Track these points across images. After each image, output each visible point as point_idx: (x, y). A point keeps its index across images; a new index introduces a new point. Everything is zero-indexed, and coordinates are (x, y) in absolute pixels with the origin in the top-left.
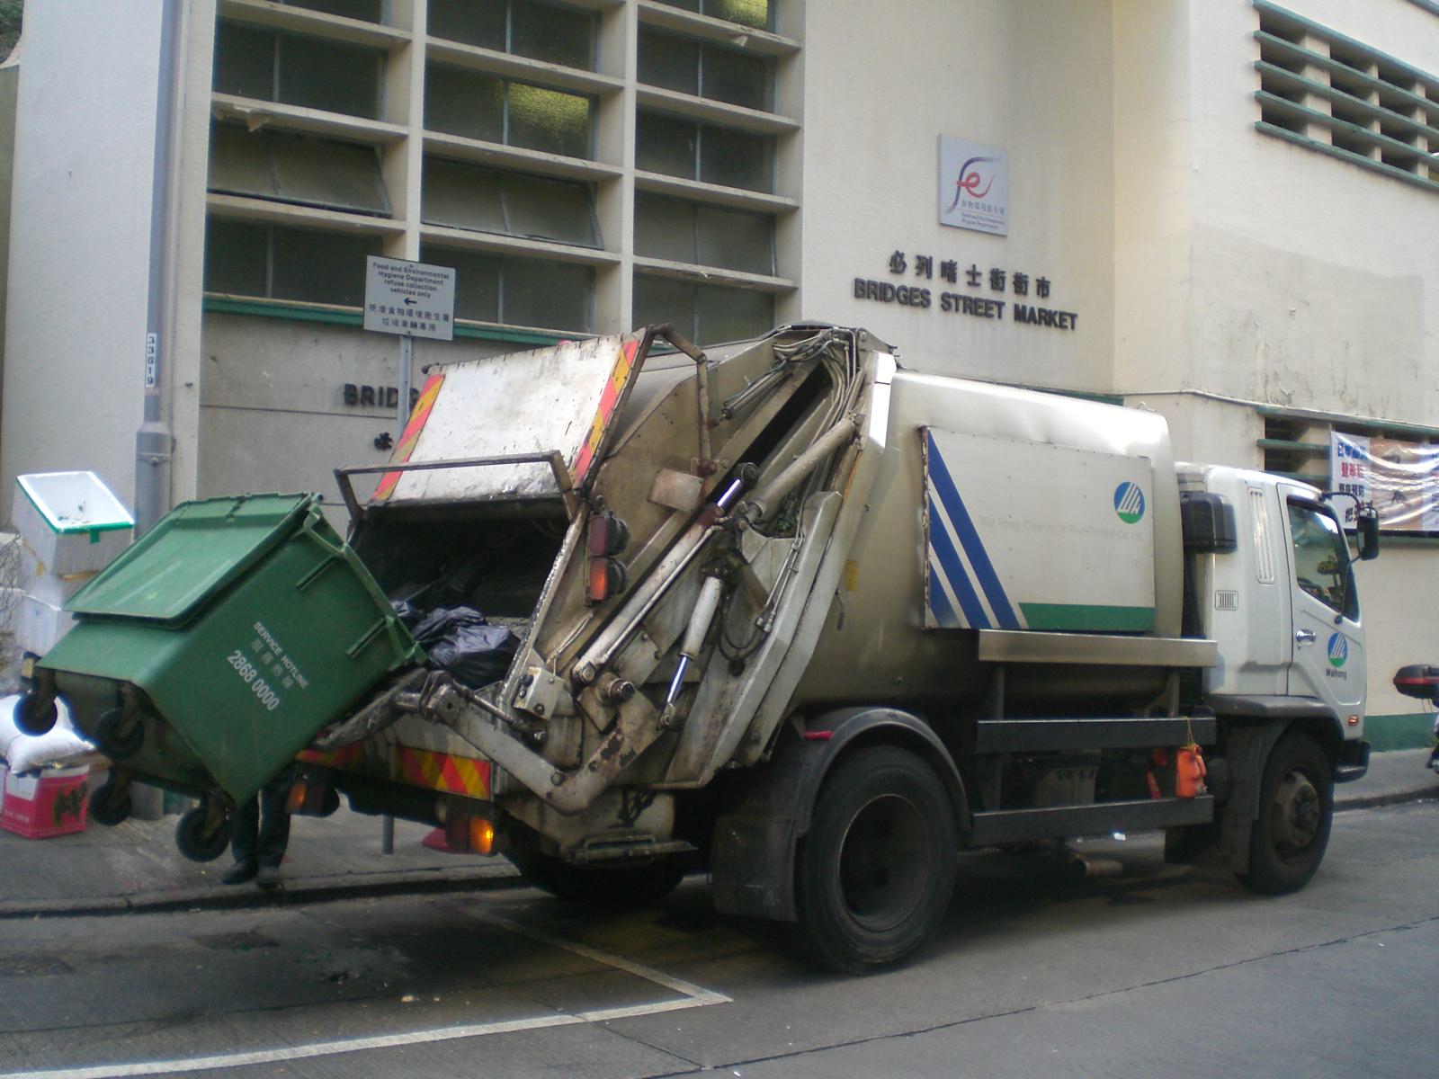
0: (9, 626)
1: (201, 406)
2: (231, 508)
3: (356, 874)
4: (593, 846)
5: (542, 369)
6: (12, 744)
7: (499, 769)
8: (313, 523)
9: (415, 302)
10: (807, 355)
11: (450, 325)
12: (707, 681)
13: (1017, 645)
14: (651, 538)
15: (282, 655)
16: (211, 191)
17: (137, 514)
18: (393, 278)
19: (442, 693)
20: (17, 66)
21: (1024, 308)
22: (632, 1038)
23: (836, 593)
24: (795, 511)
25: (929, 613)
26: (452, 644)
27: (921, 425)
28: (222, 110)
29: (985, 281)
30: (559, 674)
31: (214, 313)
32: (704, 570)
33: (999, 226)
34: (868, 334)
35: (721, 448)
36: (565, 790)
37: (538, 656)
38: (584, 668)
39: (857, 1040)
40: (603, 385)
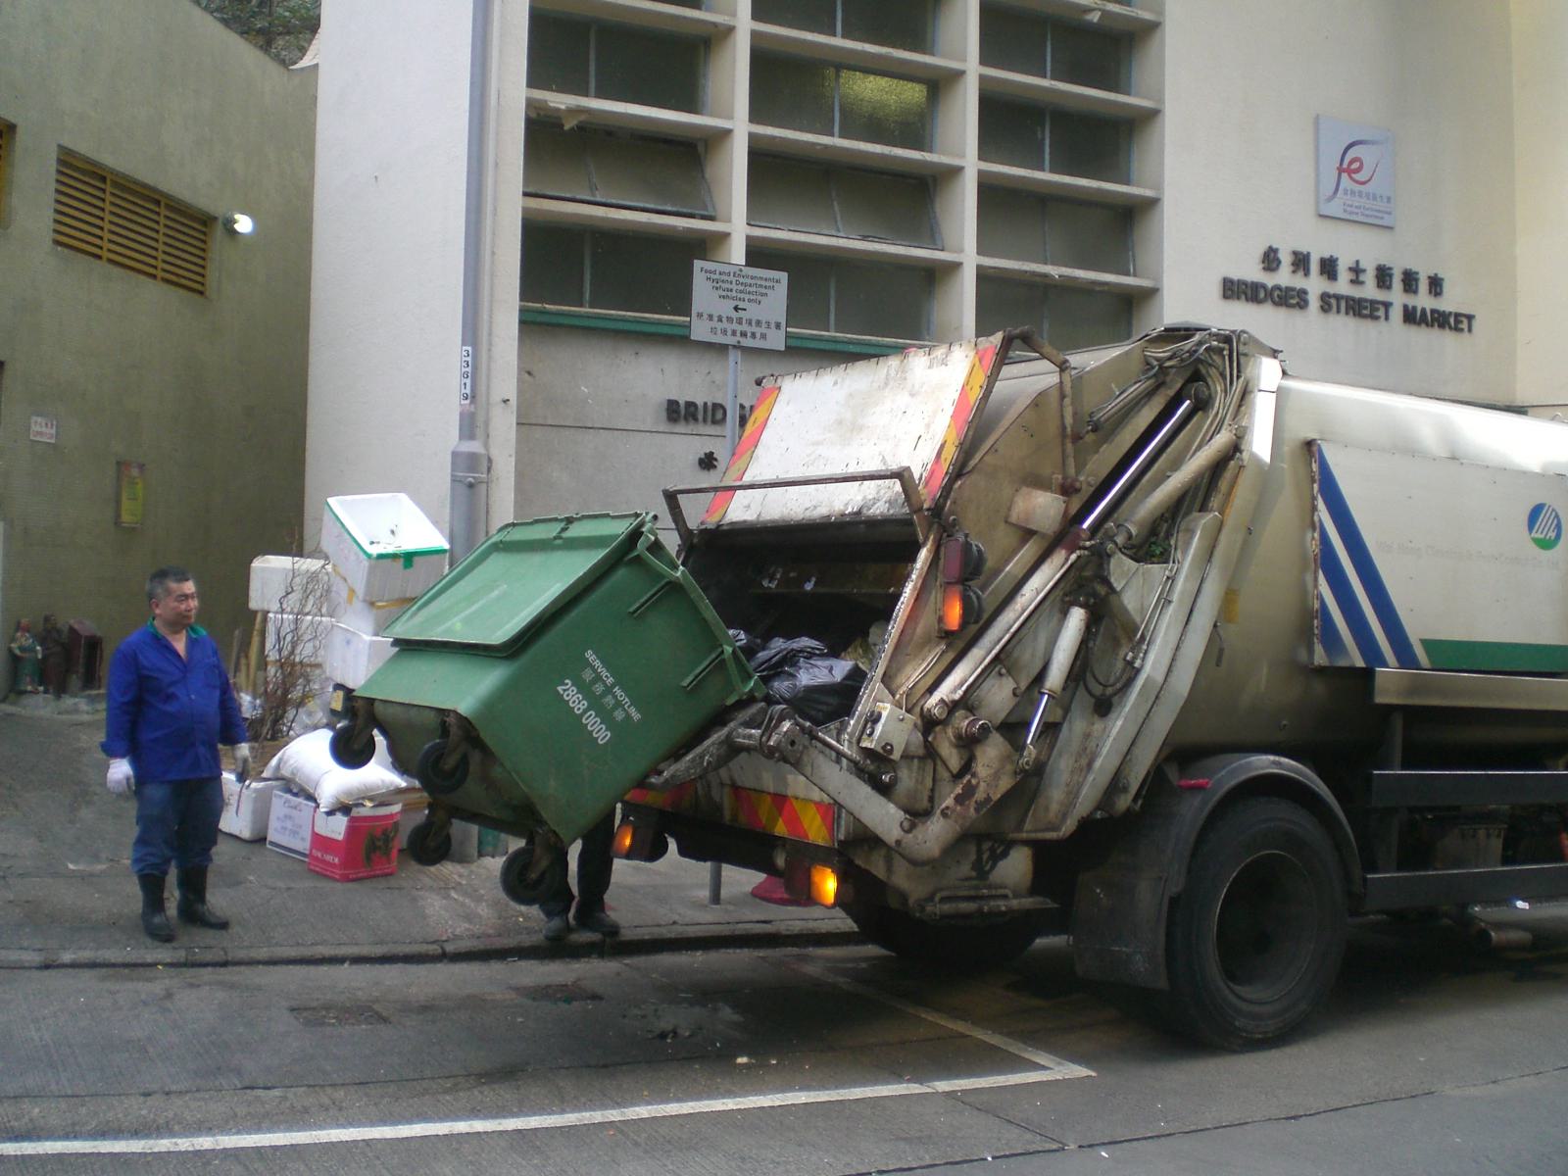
0: (316, 657)
1: (518, 424)
2: (559, 529)
3: (682, 925)
4: (944, 900)
5: (887, 379)
6: (322, 780)
7: (844, 810)
8: (647, 545)
9: (745, 310)
10: (1182, 360)
11: (782, 334)
12: (1070, 722)
13: (1416, 687)
14: (1008, 564)
15: (613, 686)
16: (526, 194)
17: (451, 541)
18: (720, 284)
19: (785, 729)
20: (317, 65)
21: (1414, 308)
22: (987, 1112)
23: (1215, 626)
24: (1168, 535)
25: (1319, 649)
26: (793, 676)
27: (1309, 439)
28: (535, 108)
29: (1370, 278)
30: (908, 711)
31: (531, 325)
32: (1067, 599)
33: (1386, 216)
34: (1251, 337)
35: (1086, 465)
36: (916, 837)
37: (886, 691)
38: (936, 705)
39: (1236, 1123)
40: (956, 396)
